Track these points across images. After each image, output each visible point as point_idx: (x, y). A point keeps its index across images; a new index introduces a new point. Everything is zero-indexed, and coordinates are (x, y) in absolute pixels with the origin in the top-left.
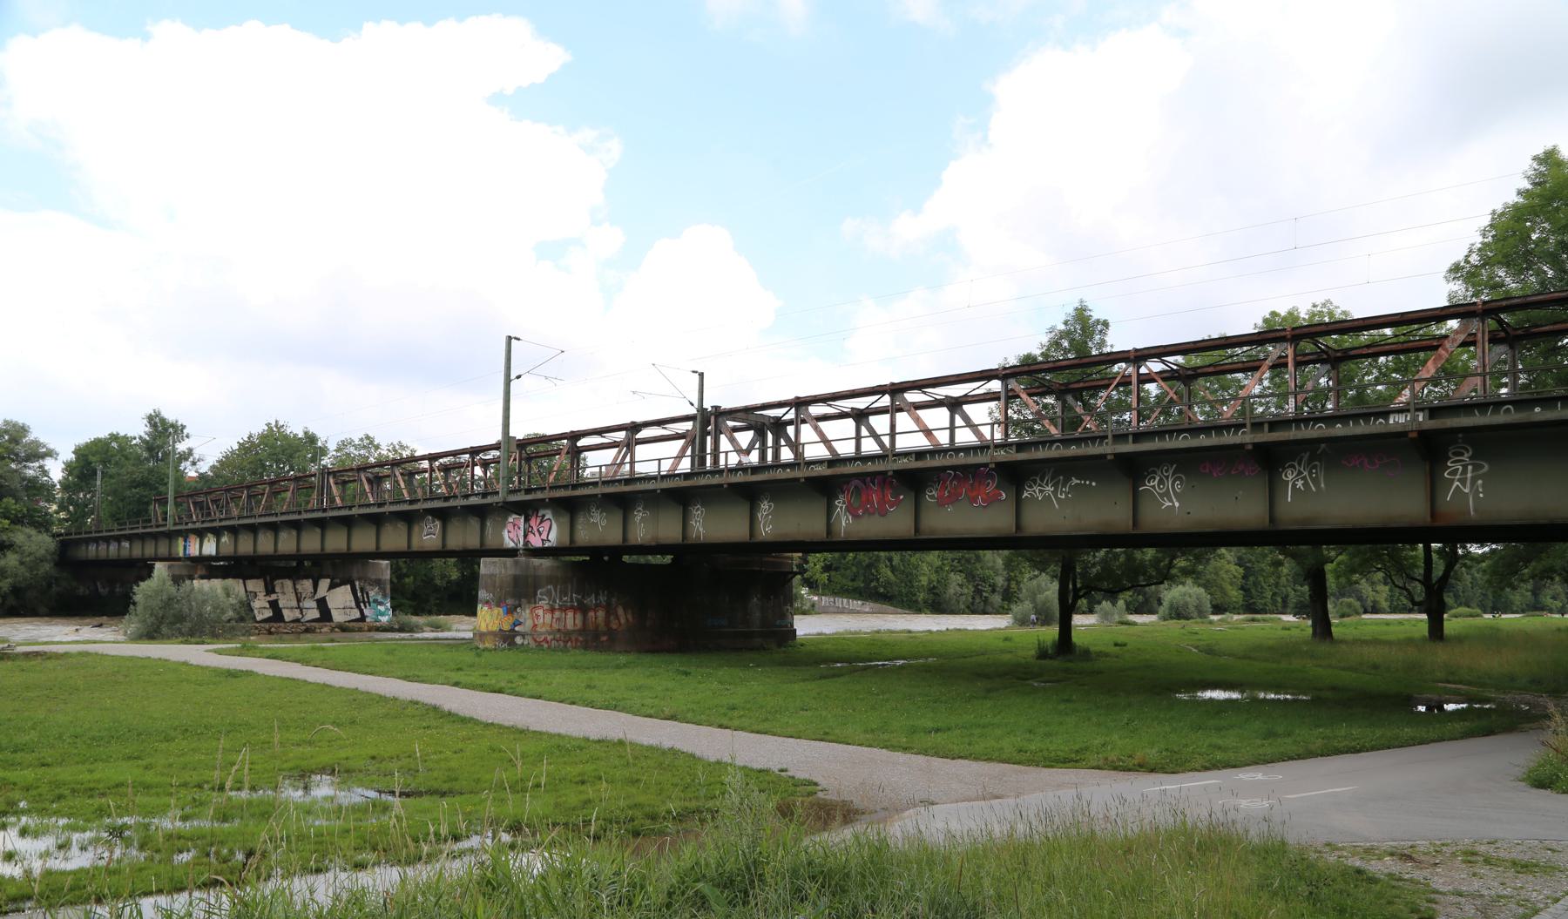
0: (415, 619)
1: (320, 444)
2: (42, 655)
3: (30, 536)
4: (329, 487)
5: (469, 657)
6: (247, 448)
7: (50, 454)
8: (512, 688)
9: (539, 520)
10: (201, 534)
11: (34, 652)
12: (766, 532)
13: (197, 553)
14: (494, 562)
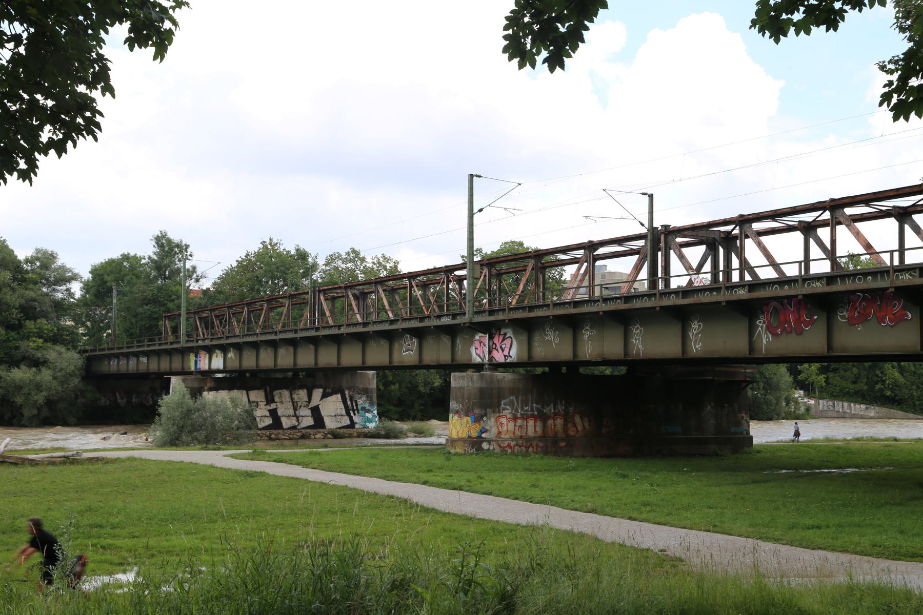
0: (399, 425)
1: (310, 260)
2: (101, 460)
3: (60, 353)
4: (320, 304)
5: (439, 460)
6: (246, 266)
7: (75, 277)
8: (469, 486)
9: (501, 338)
10: (210, 350)
11: (94, 458)
12: (697, 349)
13: (207, 368)
14: (462, 376)
